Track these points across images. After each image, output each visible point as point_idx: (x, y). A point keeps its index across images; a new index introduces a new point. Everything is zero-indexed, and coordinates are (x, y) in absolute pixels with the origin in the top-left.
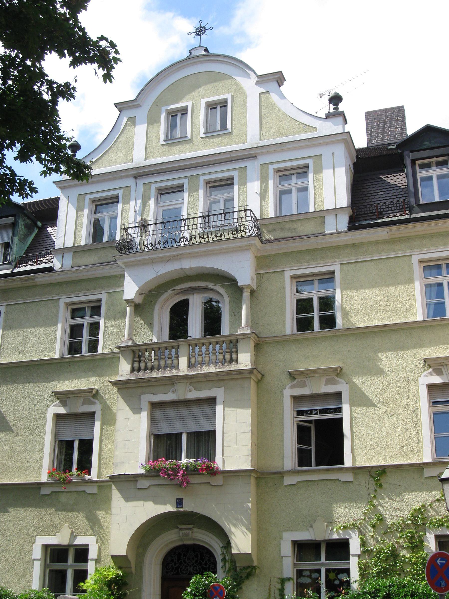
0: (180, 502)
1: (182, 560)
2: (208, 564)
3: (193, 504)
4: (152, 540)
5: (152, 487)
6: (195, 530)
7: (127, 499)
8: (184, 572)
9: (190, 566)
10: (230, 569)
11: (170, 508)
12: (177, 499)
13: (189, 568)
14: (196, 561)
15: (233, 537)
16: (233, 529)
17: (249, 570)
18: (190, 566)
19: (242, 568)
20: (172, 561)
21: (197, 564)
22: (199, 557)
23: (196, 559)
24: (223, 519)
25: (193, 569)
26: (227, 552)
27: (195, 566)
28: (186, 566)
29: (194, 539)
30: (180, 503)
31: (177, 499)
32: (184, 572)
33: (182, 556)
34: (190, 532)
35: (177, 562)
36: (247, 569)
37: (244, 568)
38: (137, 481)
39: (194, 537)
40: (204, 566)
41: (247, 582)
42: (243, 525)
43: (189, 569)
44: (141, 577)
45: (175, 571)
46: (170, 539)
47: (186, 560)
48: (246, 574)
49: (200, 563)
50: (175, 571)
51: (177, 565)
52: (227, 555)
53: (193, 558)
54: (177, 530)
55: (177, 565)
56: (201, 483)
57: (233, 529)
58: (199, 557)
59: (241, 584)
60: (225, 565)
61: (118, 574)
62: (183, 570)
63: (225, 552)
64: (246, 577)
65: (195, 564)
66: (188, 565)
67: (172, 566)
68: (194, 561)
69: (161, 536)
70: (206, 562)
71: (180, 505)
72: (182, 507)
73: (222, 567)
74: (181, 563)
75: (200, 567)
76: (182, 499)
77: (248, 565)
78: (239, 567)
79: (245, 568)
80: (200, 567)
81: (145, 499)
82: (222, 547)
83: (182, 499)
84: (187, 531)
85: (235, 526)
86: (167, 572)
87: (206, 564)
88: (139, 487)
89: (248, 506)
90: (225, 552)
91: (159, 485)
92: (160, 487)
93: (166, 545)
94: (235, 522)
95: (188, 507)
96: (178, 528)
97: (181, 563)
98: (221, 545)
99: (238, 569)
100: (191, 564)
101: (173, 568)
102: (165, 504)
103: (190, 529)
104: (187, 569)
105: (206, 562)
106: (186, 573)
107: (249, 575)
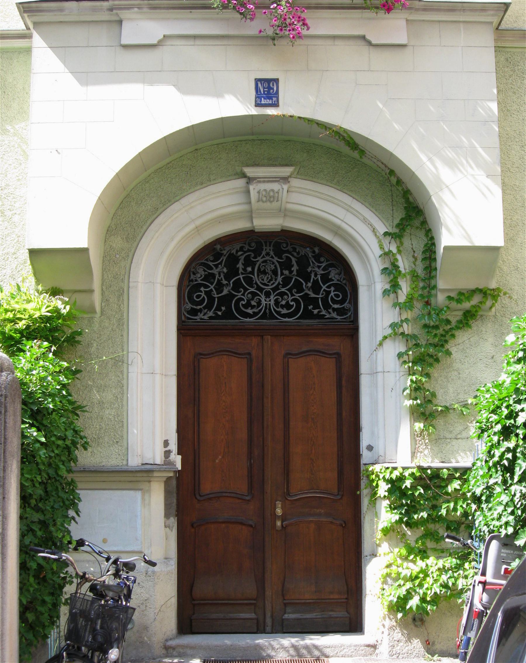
0: (270, 88)
1: (241, 276)
2: (324, 287)
3: (312, 99)
4: (155, 213)
5: (169, 42)
6: (296, 183)
7: (85, 77)
8: (250, 311)
9: (268, 294)
10: (410, 299)
11: (236, 105)
12: (257, 81)
13: (263, 298)
14: (286, 281)
15: (446, 196)
16: (446, 174)
17: (476, 300)
18: (268, 294)
19: (452, 295)
20: (209, 277)
21: (290, 290)
22: (295, 268)
23: (286, 272)
24: (415, 146)
25: (277, 303)
26: (399, 251)
27: (282, 294)
28: (254, 294)
29: (285, 213)
30: (267, 91)
31: (257, 81)
32: (250, 311)
33: (240, 266)
34: (285, 187)
35: (225, 282)
36: (469, 299)
37: (461, 293)
38: (120, 22)
39: (290, 206)
40: (313, 295)
41: (463, 337)
42: (478, 165)
43: (264, 303)
44: (122, 323)
45: (218, 309)
46: (214, 210)
47: (255, 278)
48: (460, 313)
49: (298, 287)
50: (218, 309)
51: (225, 292)
52: (399, 257)
53: (275, 272)
54: (241, 183)
55: (225, 292)
56: (334, 37)
57: (446, 174)
58: (295, 268)
59: (446, 341)
60: (395, 286)
61: (57, 310)
62: (248, 305)
63: (394, 250)
64: (460, 322)
65: (283, 290)
66: (261, 290)
67: (208, 294)
68: (280, 279)
69: (184, 201)
70: (316, 282)
71: (270, 98)
72: (276, 105)
73: (386, 293)
74: (237, 286)
75: (297, 296)
76: (276, 81)
77: (473, 287)
78: (443, 291)
79: (463, 295)
80: (297, 296)
81: (147, 77)
82: (386, 234)
83: (276, 81)
84: (275, 186)
85: (451, 164)
86: (194, 312)
87: (316, 288)
88: (125, 41)
89: (491, 110)
90: (394, 250)
91: (195, 37)
92: (198, 42)
93: (198, 230)
94: (450, 154)
95: (297, 102)
96: (244, 175)
97: (237, 286)
98: (382, 229)
99: (441, 298)
100: (268, 288)
101: (211, 300)
102: (218, 94)
103: (285, 180)
104: (259, 303)
105: (316, 282)
106: (255, 314)
107: (469, 317)
